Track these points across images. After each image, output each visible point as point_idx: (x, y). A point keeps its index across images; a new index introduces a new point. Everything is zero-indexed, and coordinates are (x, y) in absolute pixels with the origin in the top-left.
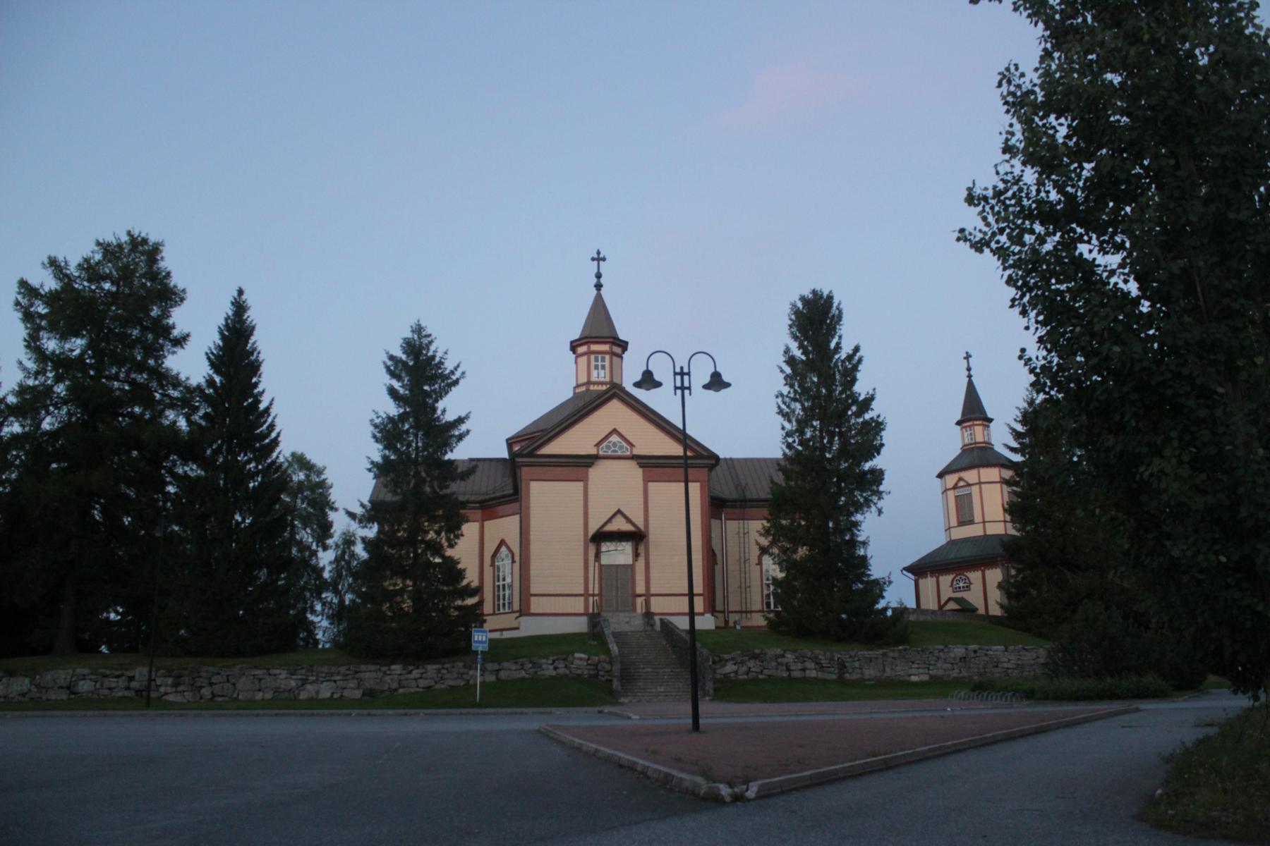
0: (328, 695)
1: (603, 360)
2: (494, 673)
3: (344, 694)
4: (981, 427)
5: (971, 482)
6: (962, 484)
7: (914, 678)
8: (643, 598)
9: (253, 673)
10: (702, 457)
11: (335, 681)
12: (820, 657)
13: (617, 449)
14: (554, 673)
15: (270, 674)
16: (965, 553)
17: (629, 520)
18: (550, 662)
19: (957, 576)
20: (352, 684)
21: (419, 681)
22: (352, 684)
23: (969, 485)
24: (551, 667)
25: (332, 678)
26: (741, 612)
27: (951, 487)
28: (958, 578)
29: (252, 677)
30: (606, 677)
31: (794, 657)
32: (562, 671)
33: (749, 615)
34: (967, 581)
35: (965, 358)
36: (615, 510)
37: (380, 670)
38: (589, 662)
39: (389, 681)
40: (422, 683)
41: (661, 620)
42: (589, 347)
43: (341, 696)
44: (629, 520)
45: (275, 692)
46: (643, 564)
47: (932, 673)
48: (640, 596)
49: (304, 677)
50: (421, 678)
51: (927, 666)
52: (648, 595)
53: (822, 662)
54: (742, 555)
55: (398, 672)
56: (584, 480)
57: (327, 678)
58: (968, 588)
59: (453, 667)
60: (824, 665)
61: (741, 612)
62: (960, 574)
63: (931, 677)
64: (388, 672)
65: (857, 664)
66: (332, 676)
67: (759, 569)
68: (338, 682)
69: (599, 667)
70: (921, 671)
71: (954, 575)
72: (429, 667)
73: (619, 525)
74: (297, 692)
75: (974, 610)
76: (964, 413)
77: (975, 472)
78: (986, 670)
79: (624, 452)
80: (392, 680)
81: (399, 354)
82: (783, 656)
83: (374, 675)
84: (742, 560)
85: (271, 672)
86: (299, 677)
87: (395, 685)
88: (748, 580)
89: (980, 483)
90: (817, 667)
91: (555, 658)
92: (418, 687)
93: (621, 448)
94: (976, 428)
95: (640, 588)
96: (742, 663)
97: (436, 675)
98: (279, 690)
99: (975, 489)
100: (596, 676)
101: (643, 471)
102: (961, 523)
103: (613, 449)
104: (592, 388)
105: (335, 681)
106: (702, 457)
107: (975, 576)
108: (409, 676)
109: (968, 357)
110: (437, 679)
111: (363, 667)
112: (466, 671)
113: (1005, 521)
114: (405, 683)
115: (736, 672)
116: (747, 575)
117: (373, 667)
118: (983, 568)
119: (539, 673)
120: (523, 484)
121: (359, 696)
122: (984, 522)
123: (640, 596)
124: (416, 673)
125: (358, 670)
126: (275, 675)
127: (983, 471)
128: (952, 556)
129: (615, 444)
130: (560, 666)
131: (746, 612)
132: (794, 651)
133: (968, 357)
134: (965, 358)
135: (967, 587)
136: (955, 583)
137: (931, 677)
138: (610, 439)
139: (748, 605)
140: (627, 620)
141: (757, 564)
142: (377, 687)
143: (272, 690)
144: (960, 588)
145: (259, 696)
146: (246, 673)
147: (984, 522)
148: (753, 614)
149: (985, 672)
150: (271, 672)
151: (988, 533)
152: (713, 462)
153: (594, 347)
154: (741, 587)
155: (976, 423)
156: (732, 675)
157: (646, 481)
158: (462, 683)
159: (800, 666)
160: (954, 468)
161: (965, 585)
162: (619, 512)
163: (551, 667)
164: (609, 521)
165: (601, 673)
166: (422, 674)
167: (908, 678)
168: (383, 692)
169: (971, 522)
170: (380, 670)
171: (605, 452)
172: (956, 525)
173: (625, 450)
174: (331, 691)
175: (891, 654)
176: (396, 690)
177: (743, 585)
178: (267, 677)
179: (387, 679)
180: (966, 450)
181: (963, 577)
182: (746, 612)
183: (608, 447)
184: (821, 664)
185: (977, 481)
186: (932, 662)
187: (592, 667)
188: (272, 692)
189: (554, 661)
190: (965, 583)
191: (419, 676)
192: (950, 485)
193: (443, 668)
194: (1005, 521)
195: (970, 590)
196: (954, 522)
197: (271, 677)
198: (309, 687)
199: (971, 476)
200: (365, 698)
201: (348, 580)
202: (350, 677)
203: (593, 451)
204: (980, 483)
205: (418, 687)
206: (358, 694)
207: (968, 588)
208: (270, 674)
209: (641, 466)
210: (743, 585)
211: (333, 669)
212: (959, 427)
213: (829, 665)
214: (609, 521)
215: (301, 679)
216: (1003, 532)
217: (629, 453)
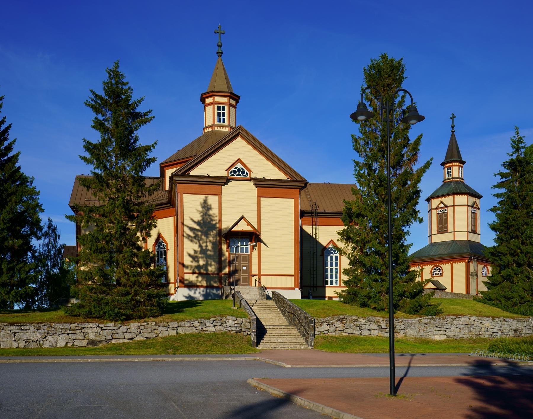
0: (63, 344)
1: (224, 109)
2: (175, 329)
3: (74, 343)
4: (457, 167)
5: (448, 205)
6: (442, 205)
7: (437, 338)
8: (257, 277)
9: (10, 328)
10: (297, 181)
11: (68, 334)
12: (380, 322)
13: (240, 173)
14: (214, 329)
15: (22, 330)
16: (441, 251)
17: (249, 224)
18: (212, 322)
19: (435, 266)
20: (80, 336)
21: (125, 334)
22: (80, 336)
23: (446, 206)
24: (212, 325)
25: (66, 333)
26: (310, 287)
27: (435, 207)
28: (435, 268)
29: (9, 332)
30: (247, 332)
31: (364, 321)
32: (219, 328)
33: (315, 288)
34: (441, 270)
35: (451, 118)
36: (240, 217)
37: (98, 326)
38: (236, 322)
39: (105, 334)
40: (127, 336)
41: (273, 293)
42: (214, 99)
43: (73, 345)
44: (249, 224)
45: (26, 342)
46: (257, 254)
47: (449, 334)
48: (255, 275)
49: (46, 331)
50: (126, 332)
51: (445, 329)
52: (260, 275)
53: (381, 325)
54: (312, 249)
55: (111, 328)
56: (219, 194)
57: (62, 332)
58: (441, 275)
59: (148, 324)
60: (383, 327)
61: (310, 287)
62: (437, 266)
63: (447, 337)
64: (105, 328)
65: (403, 327)
66: (66, 331)
67: (322, 259)
68: (70, 335)
69: (243, 326)
70: (442, 332)
71: (433, 266)
72: (132, 324)
73: (242, 227)
74: (41, 342)
75: (444, 289)
76: (446, 158)
77: (451, 198)
78: (481, 333)
79: (245, 176)
80: (107, 333)
81: (102, 93)
82: (357, 320)
83: (94, 330)
84: (312, 252)
85: (22, 327)
86: (43, 331)
87: (109, 337)
88: (315, 266)
89: (454, 206)
90: (378, 328)
91: (214, 319)
92: (125, 338)
93: (243, 172)
94: (454, 167)
95: (255, 271)
96: (332, 324)
97: (137, 330)
98: (29, 340)
99: (450, 210)
100: (240, 331)
101: (257, 189)
102: (439, 232)
103: (238, 173)
104: (216, 129)
105: (68, 334)
106: (297, 181)
107: (446, 267)
108: (119, 331)
109: (453, 117)
110: (137, 333)
111: (87, 325)
112: (156, 327)
113: (468, 232)
114: (117, 336)
115: (328, 330)
116: (315, 262)
117: (93, 325)
118: (452, 262)
119: (205, 329)
120: (179, 195)
121: (86, 345)
122: (454, 232)
123: (255, 275)
124: (123, 329)
125: (84, 326)
126: (26, 330)
127: (457, 197)
128: (432, 253)
129: (239, 170)
130: (218, 324)
131: (314, 287)
132: (364, 318)
133: (453, 117)
134: (451, 118)
135: (441, 274)
136: (433, 271)
137: (447, 337)
138: (236, 166)
139: (315, 283)
140: (248, 291)
141: (321, 255)
142: (97, 339)
143: (24, 340)
144: (436, 274)
145: (15, 345)
146: (5, 329)
147: (454, 232)
148: (318, 288)
149: (479, 334)
150: (22, 327)
151: (456, 239)
152: (303, 185)
153: (218, 99)
154: (310, 270)
155: (454, 164)
156: (326, 332)
157: (259, 196)
158: (155, 336)
159: (368, 327)
160: (437, 195)
161: (440, 272)
162: (243, 218)
163: (212, 325)
164: (236, 224)
165: (244, 330)
166: (127, 329)
167: (433, 337)
168: (101, 342)
169: (446, 231)
170: (98, 326)
171: (232, 175)
172: (436, 233)
173: (245, 174)
174: (66, 341)
175: (424, 321)
176: (110, 340)
177: (312, 269)
178: (20, 331)
179: (104, 333)
180: (446, 183)
181: (439, 268)
182: (314, 287)
183: (235, 172)
184: (381, 326)
185: (453, 204)
186: (448, 327)
187: (239, 325)
188: (25, 342)
189: (213, 321)
190: (439, 271)
191: (125, 331)
192: (434, 206)
193: (141, 325)
194: (468, 232)
195: (442, 276)
196: (434, 231)
197: (22, 331)
198: (50, 338)
199: (448, 200)
200: (89, 346)
201: (395, 207)
202: (78, 331)
203: (225, 174)
204: (454, 206)
205: (125, 338)
206: (84, 343)
207: (441, 275)
208: (22, 330)
209: (257, 185)
210: (312, 269)
211: (67, 326)
212: (443, 167)
213: (385, 327)
214: (236, 224)
215: (44, 333)
216: (466, 239)
217: (248, 177)
